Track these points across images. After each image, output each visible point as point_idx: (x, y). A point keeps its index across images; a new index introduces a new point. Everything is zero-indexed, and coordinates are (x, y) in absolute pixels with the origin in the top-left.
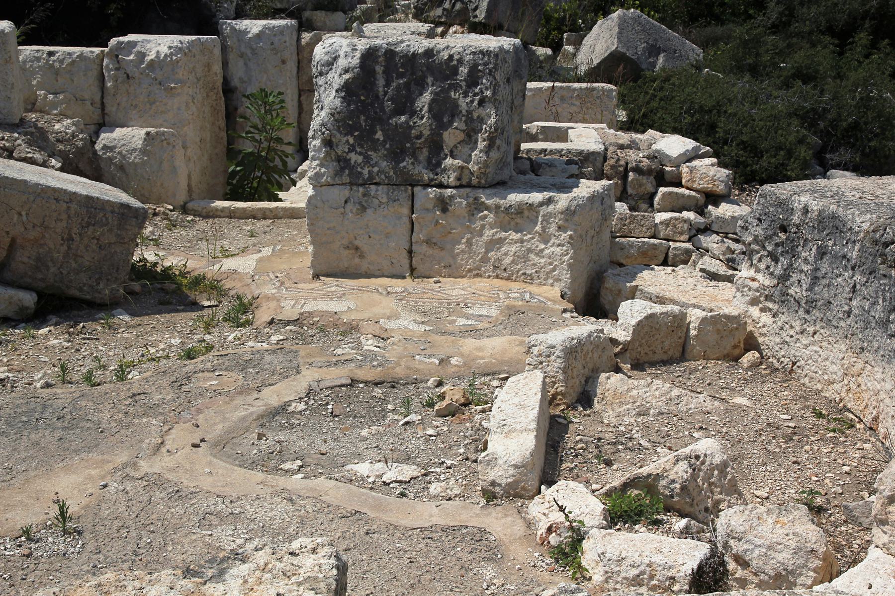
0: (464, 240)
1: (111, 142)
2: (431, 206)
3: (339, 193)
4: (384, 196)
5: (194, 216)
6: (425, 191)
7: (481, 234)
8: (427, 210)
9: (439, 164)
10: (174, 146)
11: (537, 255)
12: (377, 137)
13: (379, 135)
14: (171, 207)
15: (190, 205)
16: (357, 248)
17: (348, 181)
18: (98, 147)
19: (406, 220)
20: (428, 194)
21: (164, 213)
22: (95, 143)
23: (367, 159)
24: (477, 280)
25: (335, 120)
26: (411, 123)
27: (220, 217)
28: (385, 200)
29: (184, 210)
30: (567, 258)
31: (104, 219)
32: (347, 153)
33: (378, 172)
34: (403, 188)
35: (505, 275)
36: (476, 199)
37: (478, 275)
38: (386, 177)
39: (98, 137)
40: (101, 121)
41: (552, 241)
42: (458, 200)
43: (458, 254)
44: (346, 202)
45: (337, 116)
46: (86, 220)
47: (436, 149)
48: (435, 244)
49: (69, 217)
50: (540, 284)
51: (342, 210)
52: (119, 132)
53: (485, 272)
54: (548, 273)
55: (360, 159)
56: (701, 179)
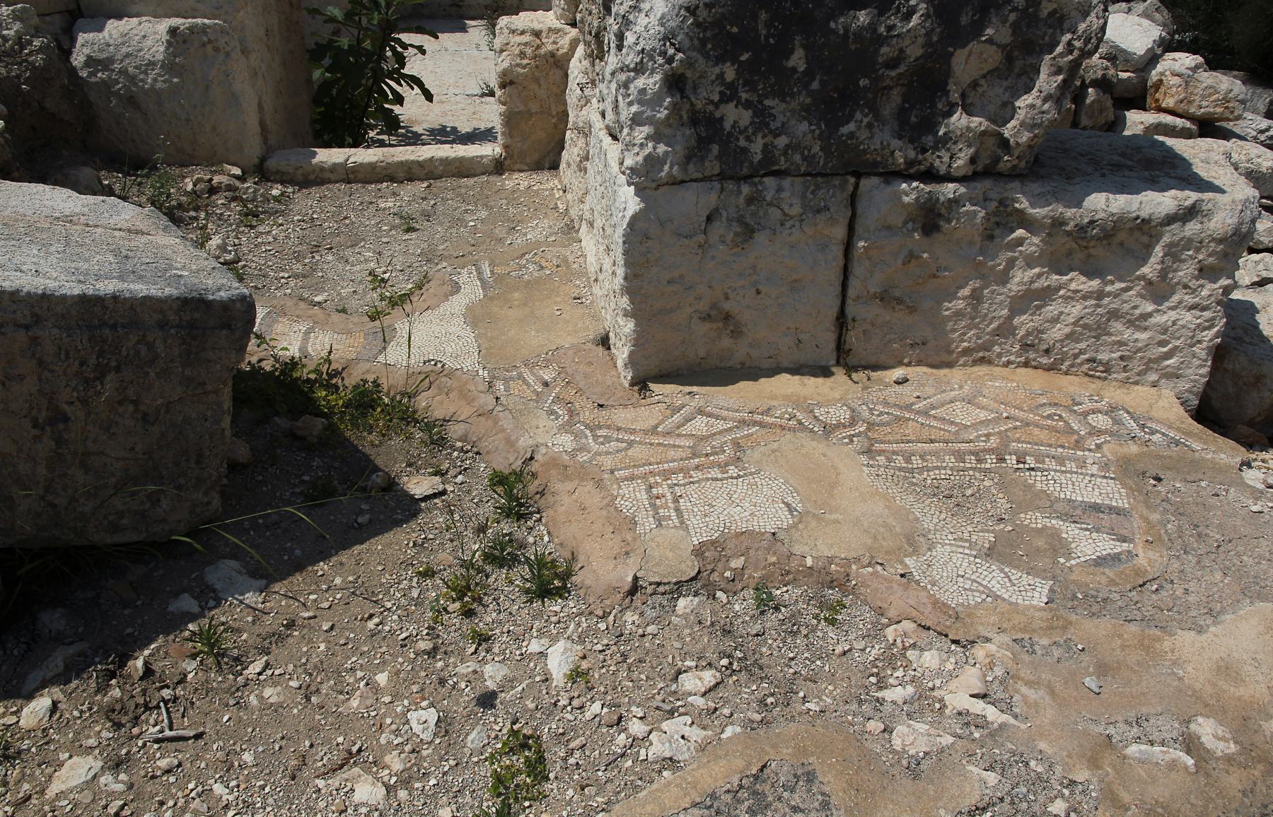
0: (966, 291)
1: (101, 51)
2: (897, 220)
3: (693, 202)
4: (797, 202)
5: (282, 183)
6: (889, 189)
7: (1004, 279)
8: (889, 228)
9: (929, 125)
10: (228, 55)
11: (1131, 323)
12: (791, 64)
13: (798, 60)
14: (237, 171)
15: (272, 164)
16: (727, 317)
17: (716, 171)
18: (78, 59)
19: (837, 251)
20: (897, 196)
21: (230, 188)
22: (69, 53)
23: (762, 119)
24: (981, 370)
25: (697, 24)
26: (882, 29)
27: (330, 182)
28: (796, 210)
29: (262, 172)
30: (1209, 334)
31: (143, 350)
32: (717, 105)
33: (788, 146)
34: (836, 181)
35: (1044, 360)
36: (1002, 203)
37: (982, 361)
38: (804, 158)
39: (73, 40)
40: (73, 6)
41: (1176, 298)
42: (968, 207)
43: (949, 318)
44: (709, 219)
45: (703, 14)
46: (92, 361)
47: (927, 93)
48: (900, 301)
49: (41, 363)
50: (1126, 382)
51: (701, 238)
52: (114, 29)
53: (1000, 355)
54: (1150, 360)
55: (745, 117)
56: (1203, 97)
